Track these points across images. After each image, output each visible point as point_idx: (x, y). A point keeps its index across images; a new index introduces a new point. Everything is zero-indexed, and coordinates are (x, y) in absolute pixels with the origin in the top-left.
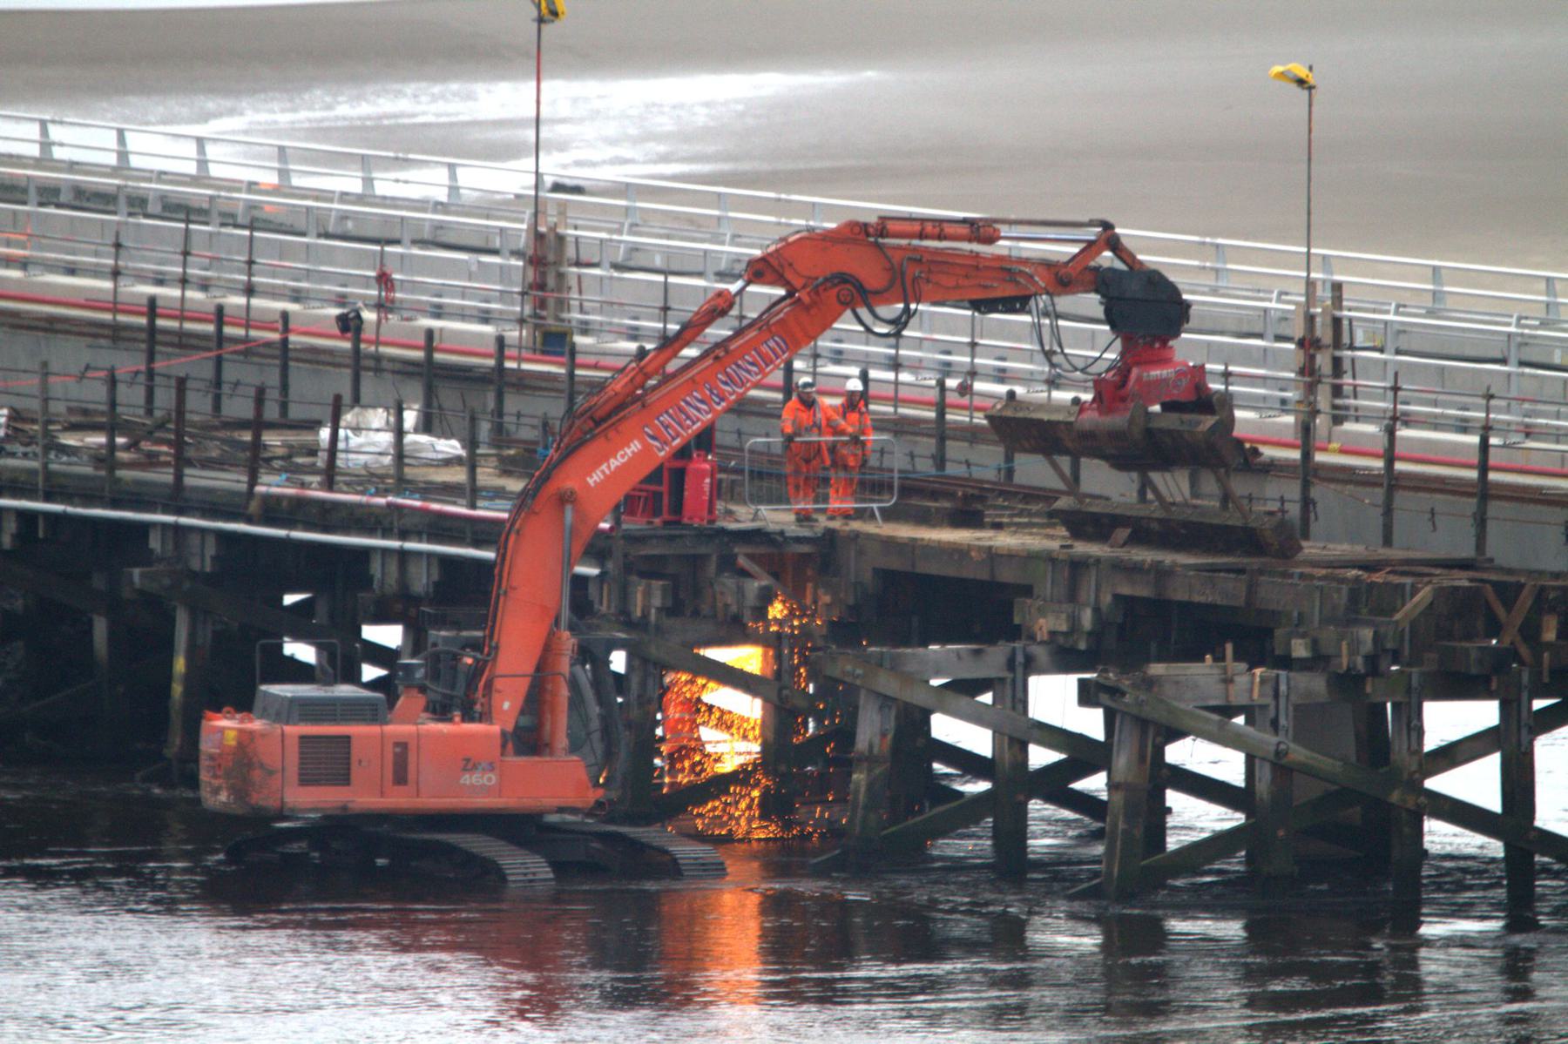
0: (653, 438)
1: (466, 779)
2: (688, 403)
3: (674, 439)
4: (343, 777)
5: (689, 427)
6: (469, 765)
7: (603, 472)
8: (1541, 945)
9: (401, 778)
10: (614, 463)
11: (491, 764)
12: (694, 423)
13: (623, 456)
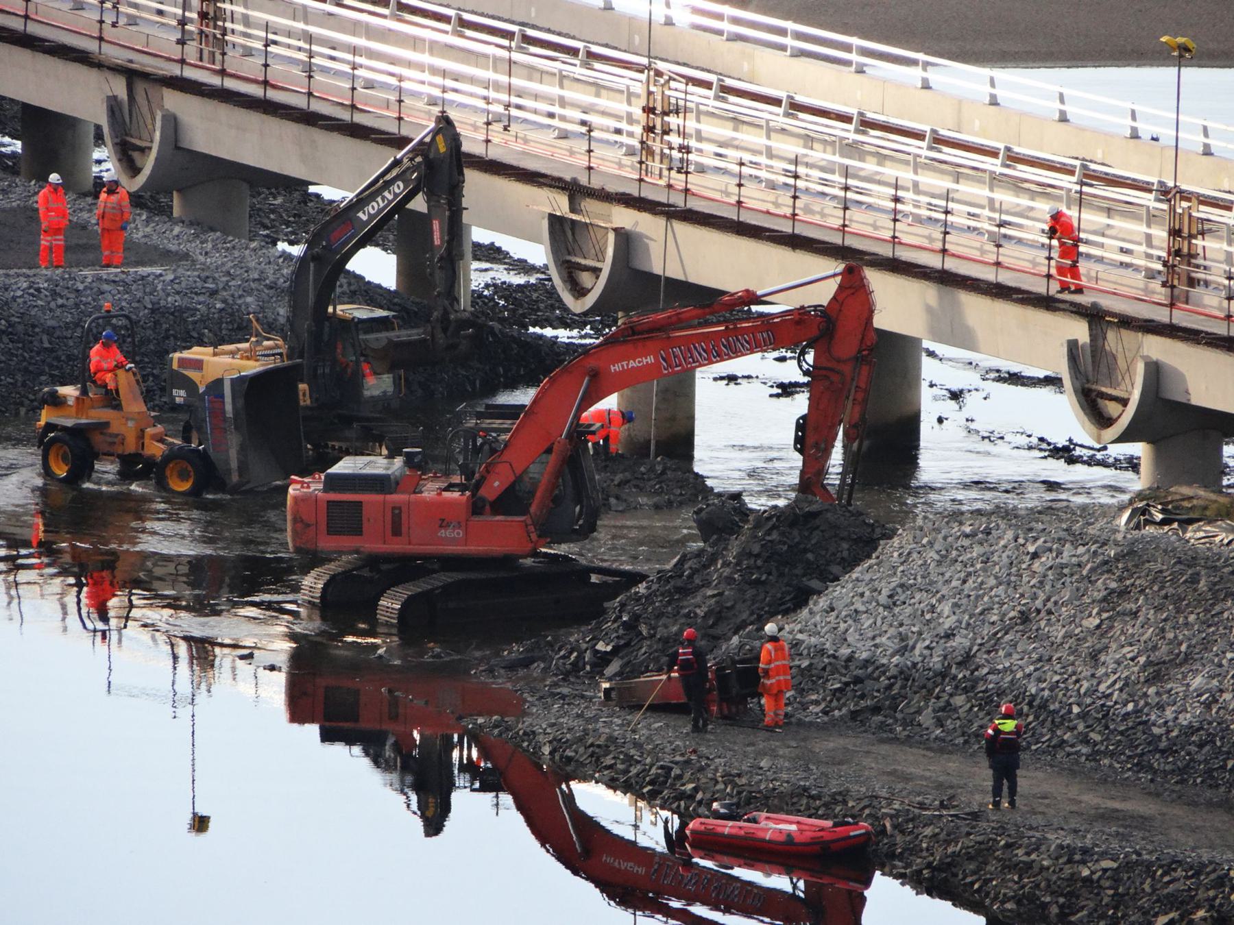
0: (664, 359)
1: (442, 533)
2: (695, 348)
3: (677, 366)
4: (356, 529)
5: (690, 363)
6: (443, 524)
7: (623, 366)
8: (439, 494)
9: (397, 532)
10: (632, 364)
11: (459, 523)
12: (694, 362)
13: (639, 362)
